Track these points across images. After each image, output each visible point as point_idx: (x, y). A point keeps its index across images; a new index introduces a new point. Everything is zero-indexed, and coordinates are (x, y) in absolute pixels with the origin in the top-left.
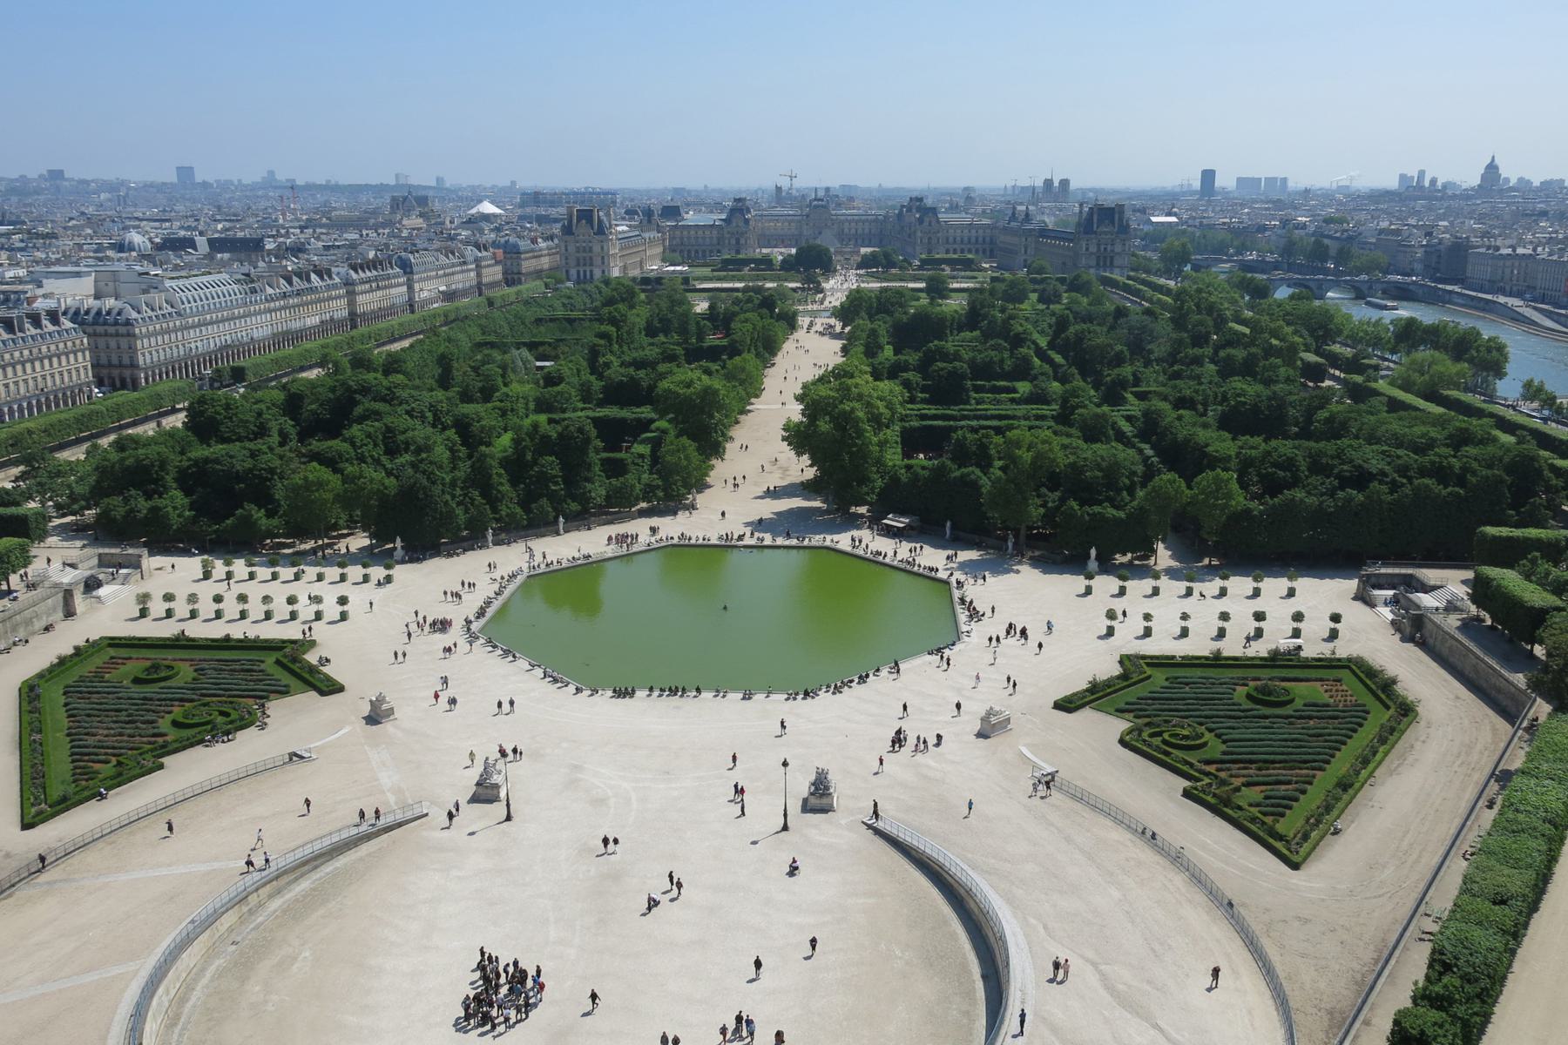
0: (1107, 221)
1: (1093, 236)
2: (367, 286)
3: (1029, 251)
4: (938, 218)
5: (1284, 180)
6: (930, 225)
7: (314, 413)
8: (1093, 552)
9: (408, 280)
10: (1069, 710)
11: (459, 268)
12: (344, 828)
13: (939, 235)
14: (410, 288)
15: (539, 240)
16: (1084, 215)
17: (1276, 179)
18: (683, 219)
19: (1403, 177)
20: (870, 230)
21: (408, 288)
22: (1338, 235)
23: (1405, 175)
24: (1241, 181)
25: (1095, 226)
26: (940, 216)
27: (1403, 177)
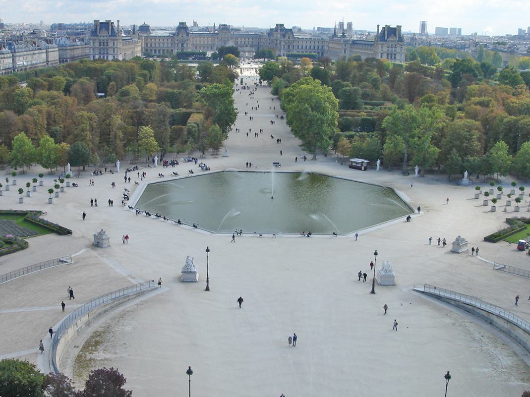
0: (392, 35)
1: (385, 43)
3: (346, 51)
4: (293, 36)
5: (460, 30)
6: (289, 38)
7: (119, 124)
8: (378, 162)
9: (13, 55)
10: (494, 242)
11: (37, 52)
12: (97, 299)
13: (294, 44)
14: (13, 57)
15: (77, 40)
16: (380, 31)
17: (456, 28)
18: (151, 33)
19: (520, 30)
20: (252, 42)
21: (13, 60)
22: (505, 50)
23: (521, 29)
24: (438, 29)
25: (386, 37)
26: (294, 34)
27: (520, 30)
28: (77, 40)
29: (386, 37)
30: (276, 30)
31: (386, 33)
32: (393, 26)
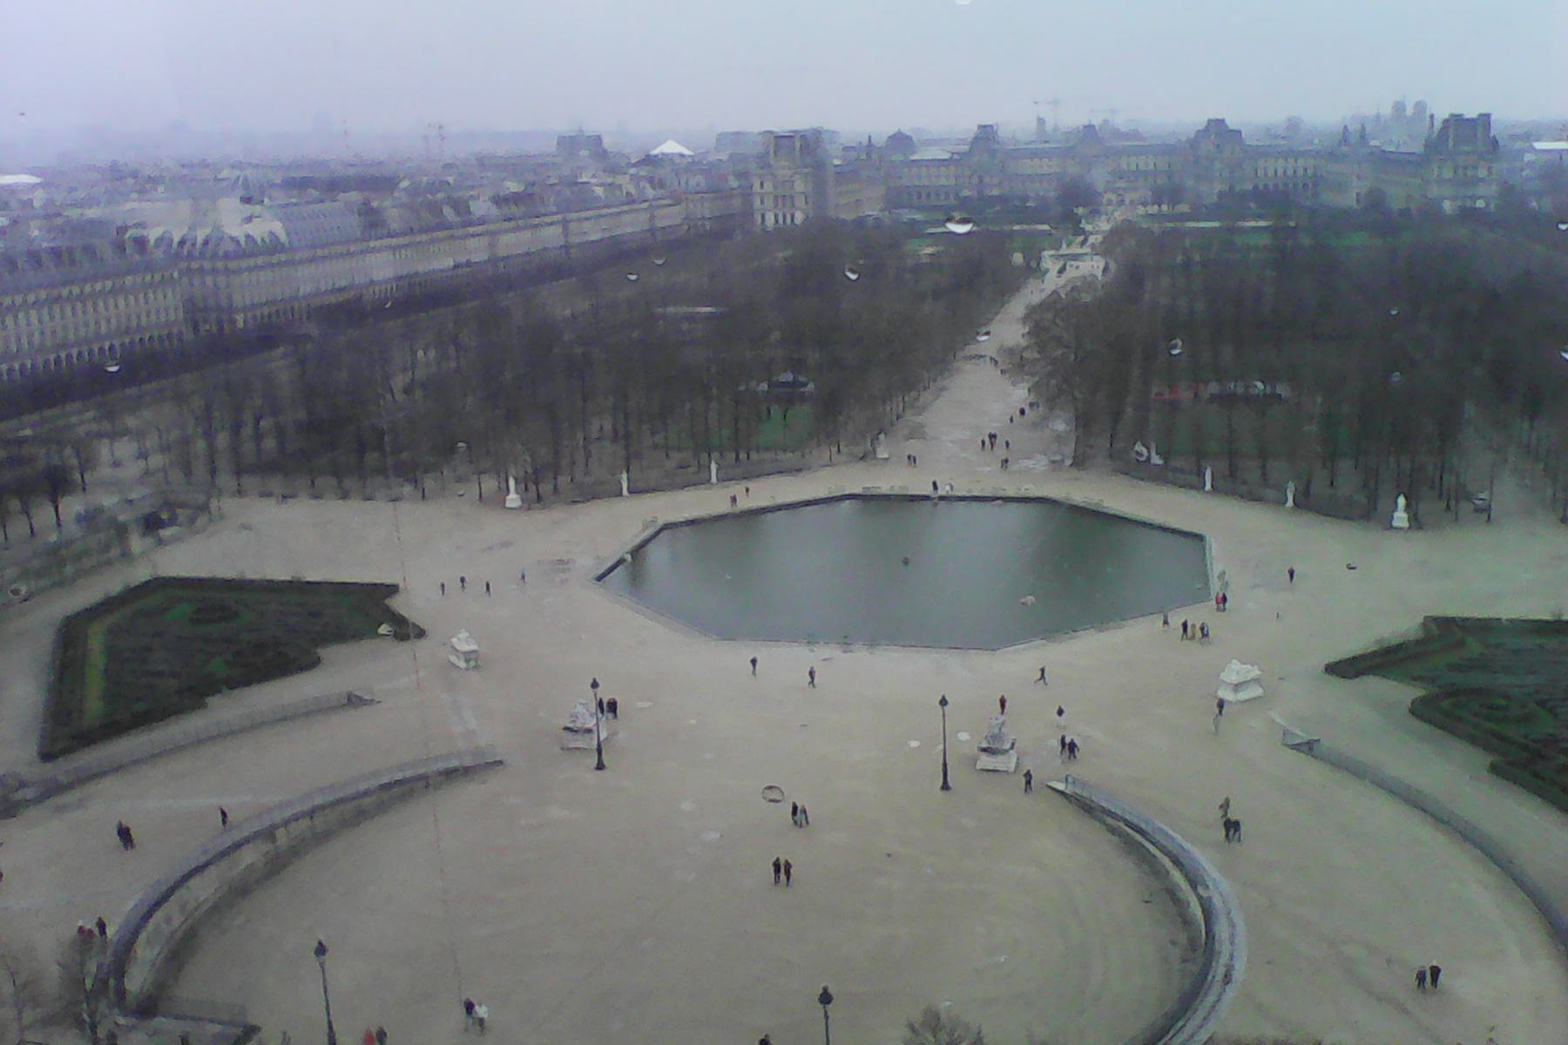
2: (512, 224)
11: (626, 208)
25: (1451, 143)
28: (731, 178)
29: (1451, 143)
30: (1207, 129)
31: (1451, 133)
32: (1471, 113)
